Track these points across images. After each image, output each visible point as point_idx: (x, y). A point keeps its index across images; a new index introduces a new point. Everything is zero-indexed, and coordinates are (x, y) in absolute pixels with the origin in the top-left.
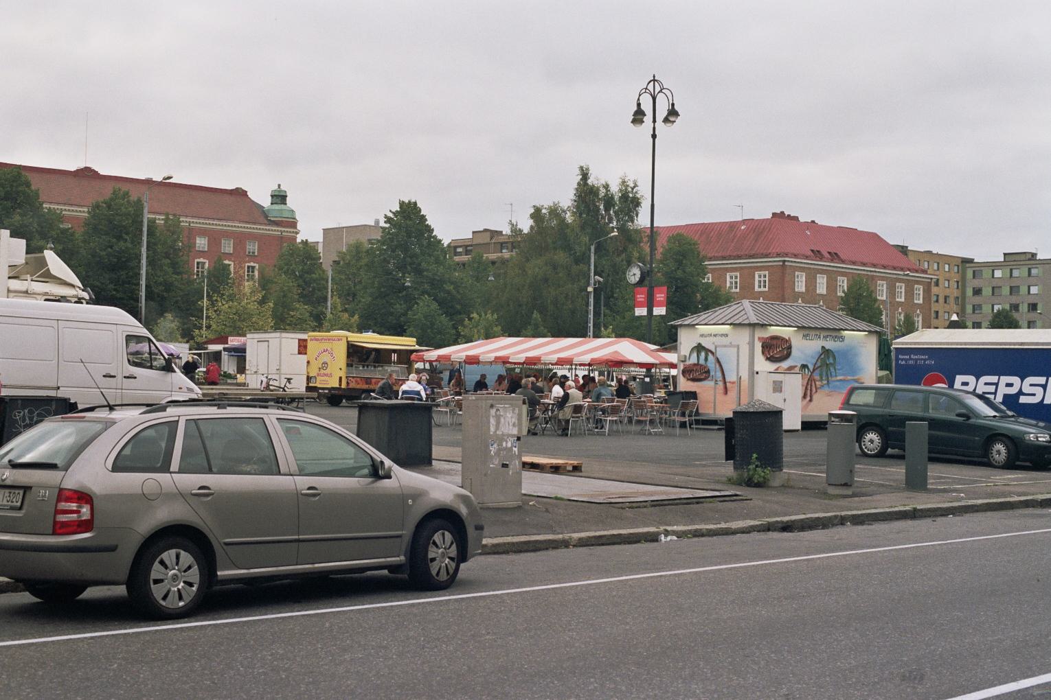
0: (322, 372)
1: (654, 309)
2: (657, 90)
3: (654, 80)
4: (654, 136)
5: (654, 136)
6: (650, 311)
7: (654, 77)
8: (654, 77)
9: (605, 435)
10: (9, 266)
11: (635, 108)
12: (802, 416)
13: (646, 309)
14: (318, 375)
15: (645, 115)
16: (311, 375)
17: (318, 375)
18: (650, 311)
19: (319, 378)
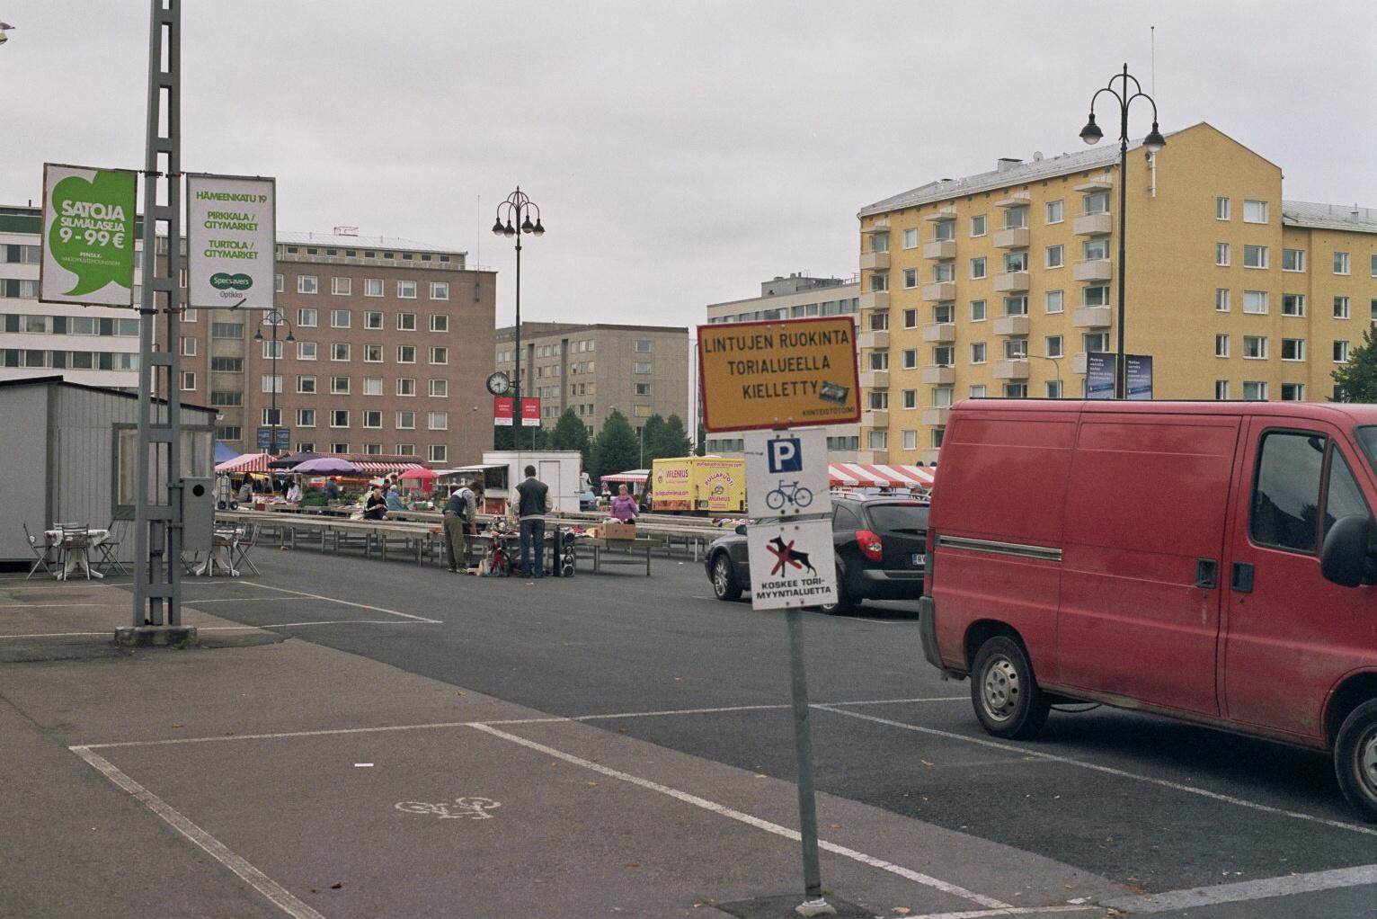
0: (716, 495)
1: (523, 419)
2: (1130, 93)
3: (518, 192)
4: (518, 248)
5: (518, 248)
6: (517, 421)
7: (1125, 67)
8: (1125, 67)
9: (693, 560)
10: (708, 307)
11: (495, 223)
12: (835, 539)
13: (511, 419)
14: (710, 499)
15: (1102, 136)
16: (700, 499)
17: (710, 499)
18: (517, 421)
19: (710, 503)
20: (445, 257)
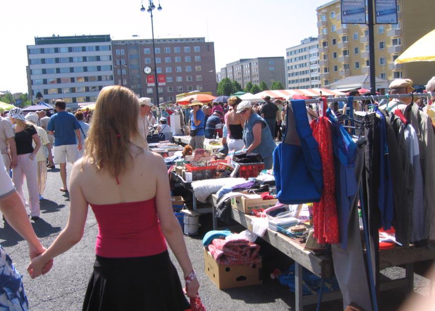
20: (199, 39)
